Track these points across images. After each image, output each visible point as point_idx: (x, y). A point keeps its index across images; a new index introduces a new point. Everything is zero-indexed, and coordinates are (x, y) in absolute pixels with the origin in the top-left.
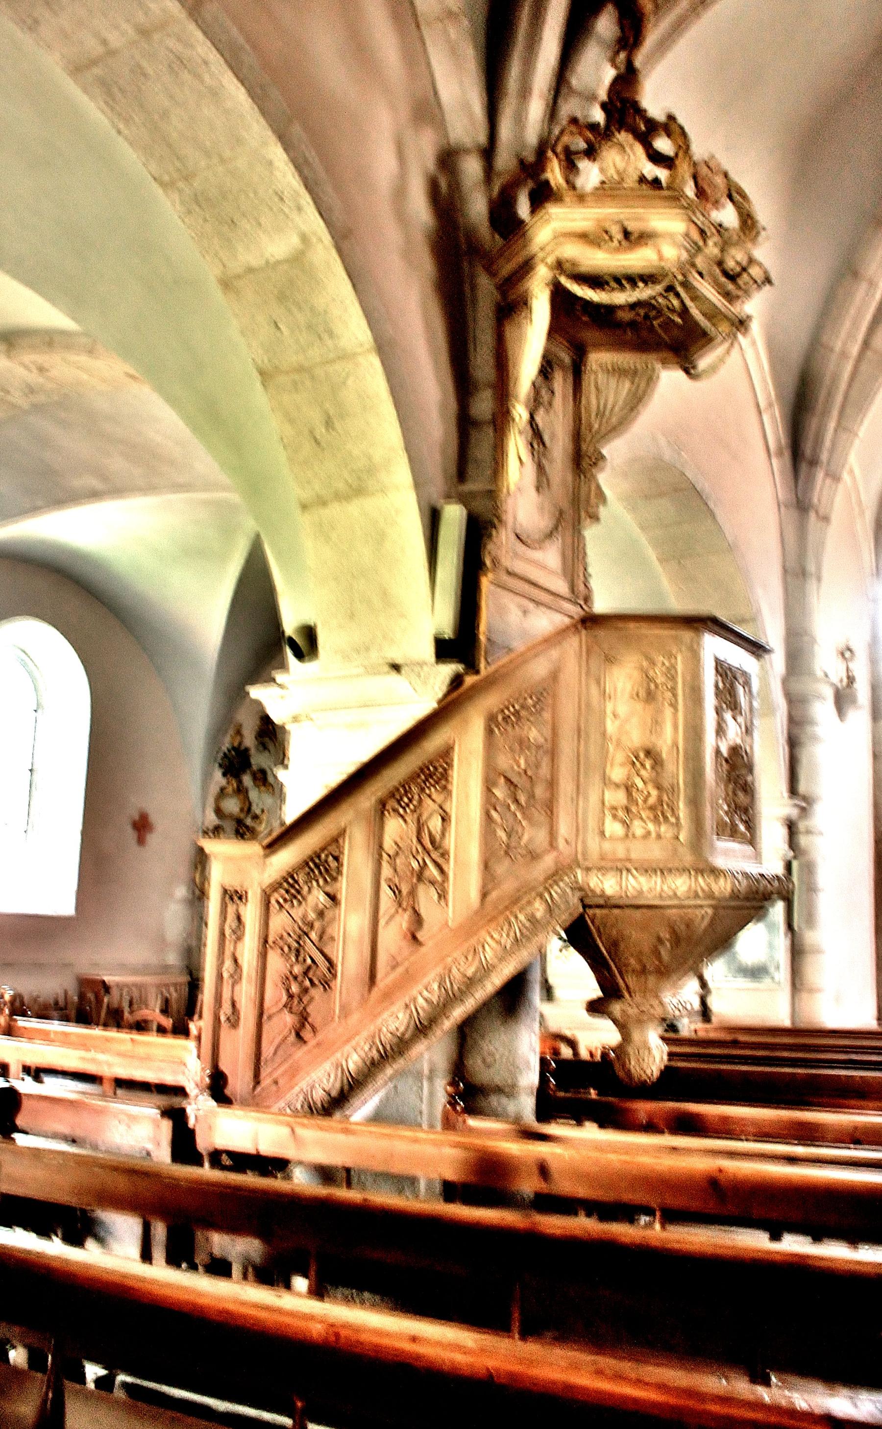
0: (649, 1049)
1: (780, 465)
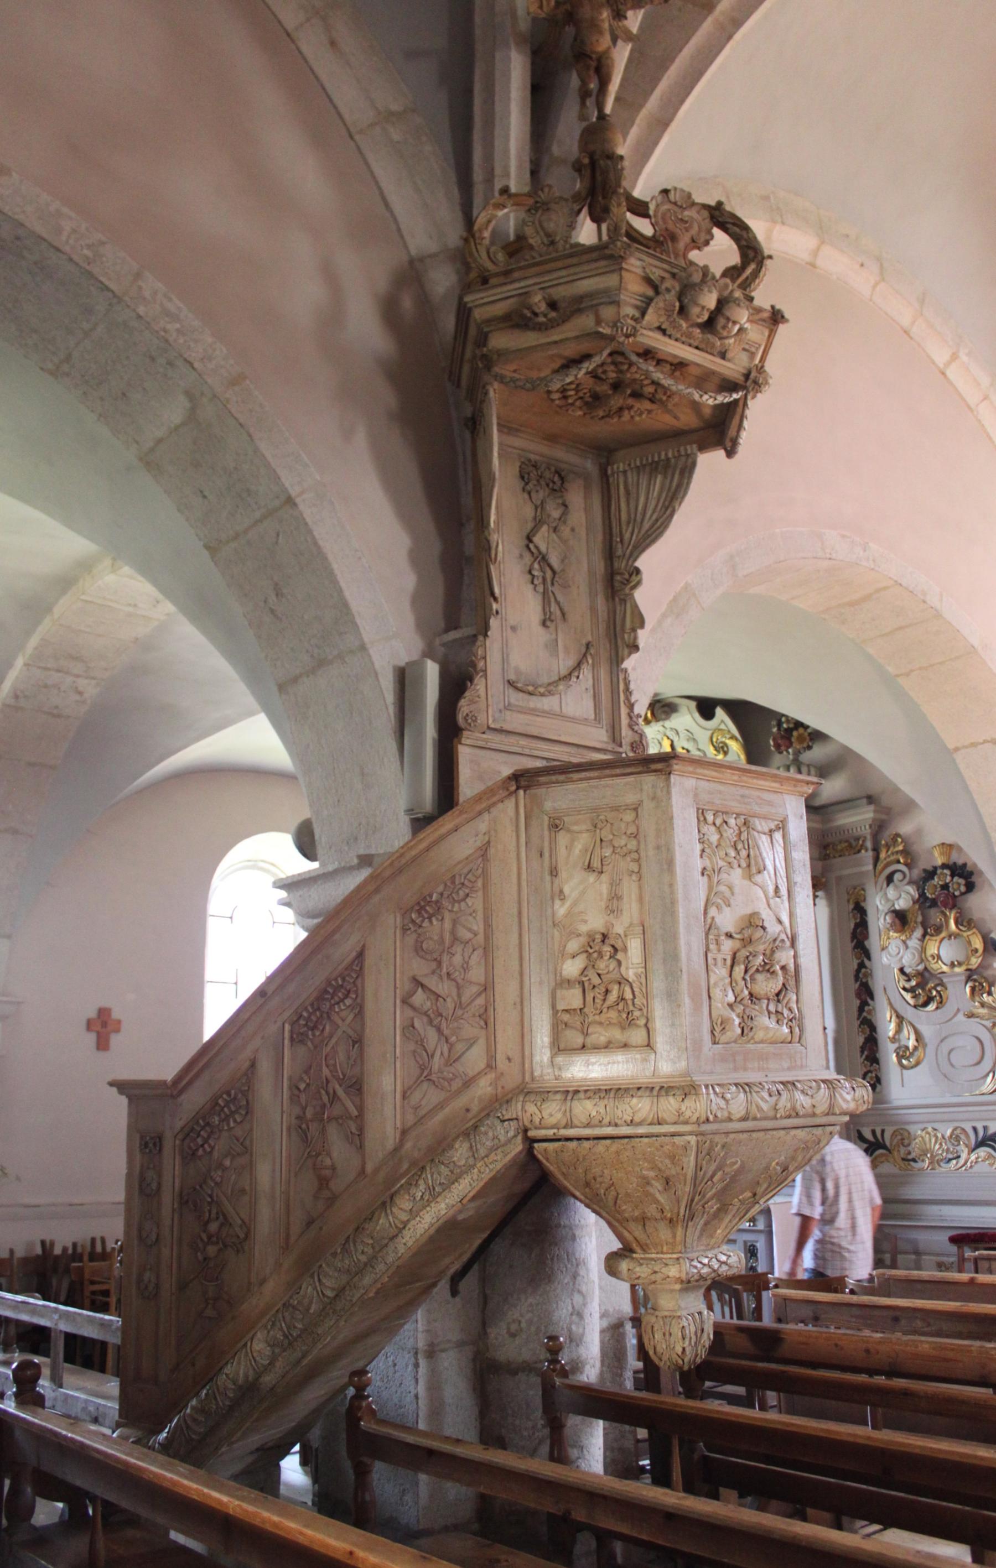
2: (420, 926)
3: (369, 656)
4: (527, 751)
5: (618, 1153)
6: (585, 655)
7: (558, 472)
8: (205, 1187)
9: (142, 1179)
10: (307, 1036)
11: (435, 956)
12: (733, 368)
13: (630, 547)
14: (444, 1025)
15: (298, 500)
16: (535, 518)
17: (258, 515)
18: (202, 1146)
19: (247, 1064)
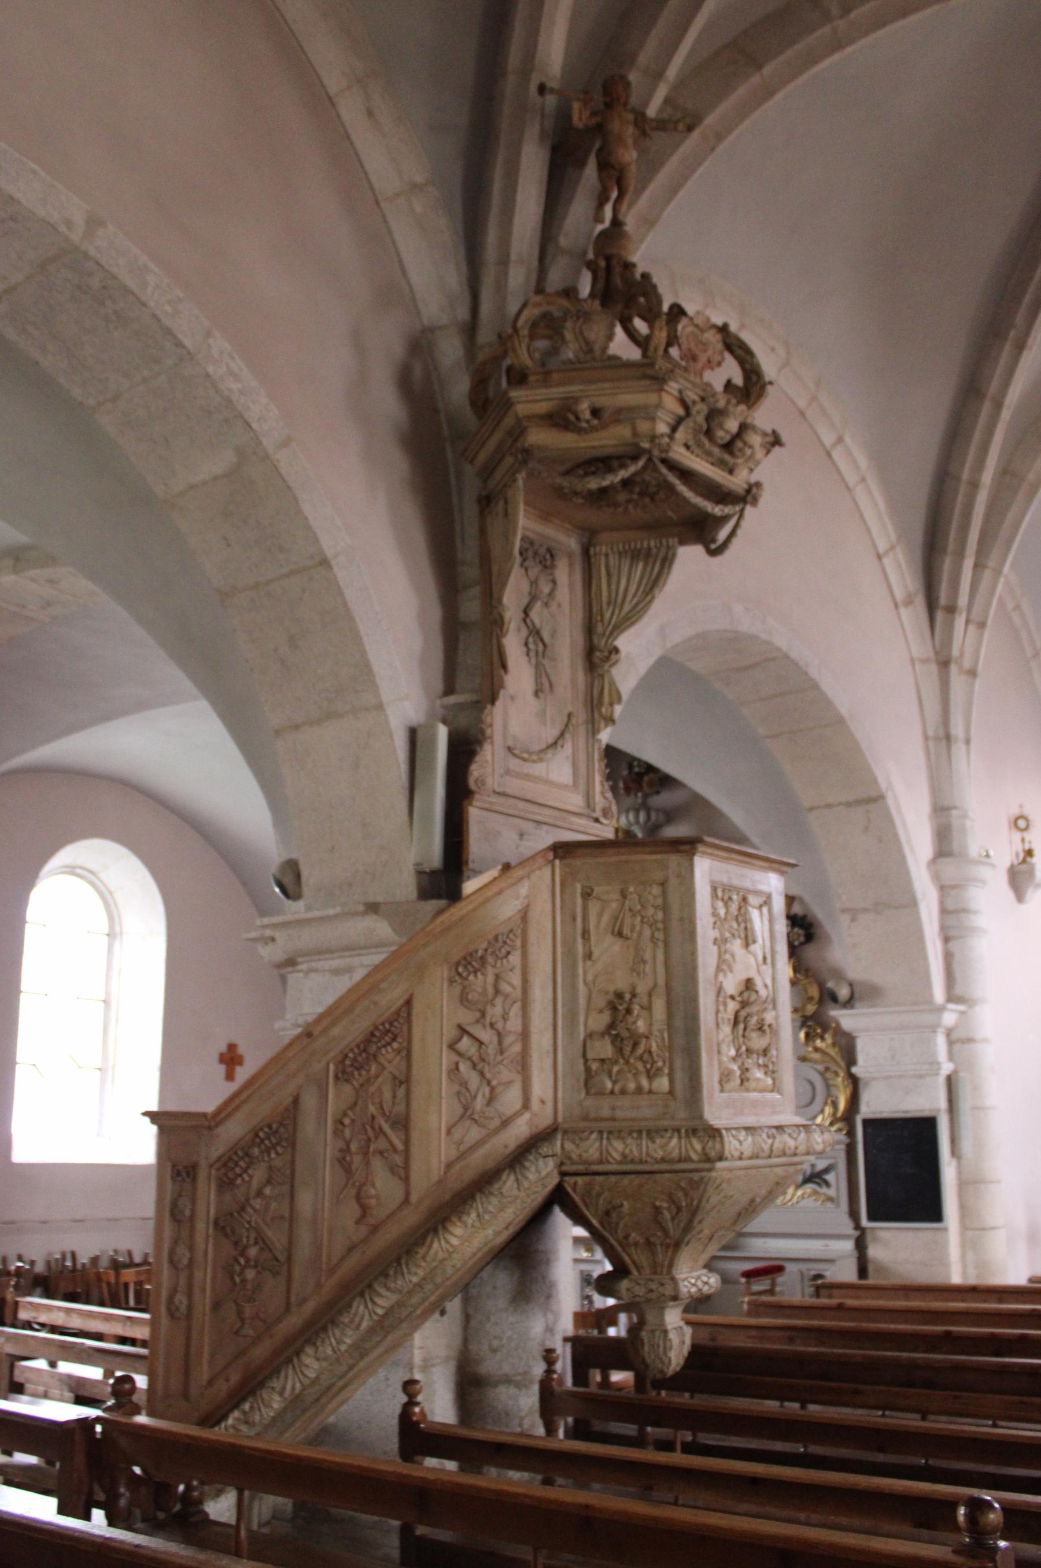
0: (665, 1332)
1: (914, 615)
2: (466, 979)
3: (386, 716)
4: (522, 814)
5: (641, 1186)
6: (567, 726)
7: (549, 550)
8: (244, 1215)
9: (174, 1205)
10: (353, 1075)
11: (479, 1006)
12: (737, 482)
13: (611, 627)
14: (486, 1070)
15: (333, 563)
16: (530, 593)
17: (285, 570)
18: (240, 1175)
19: (290, 1099)
